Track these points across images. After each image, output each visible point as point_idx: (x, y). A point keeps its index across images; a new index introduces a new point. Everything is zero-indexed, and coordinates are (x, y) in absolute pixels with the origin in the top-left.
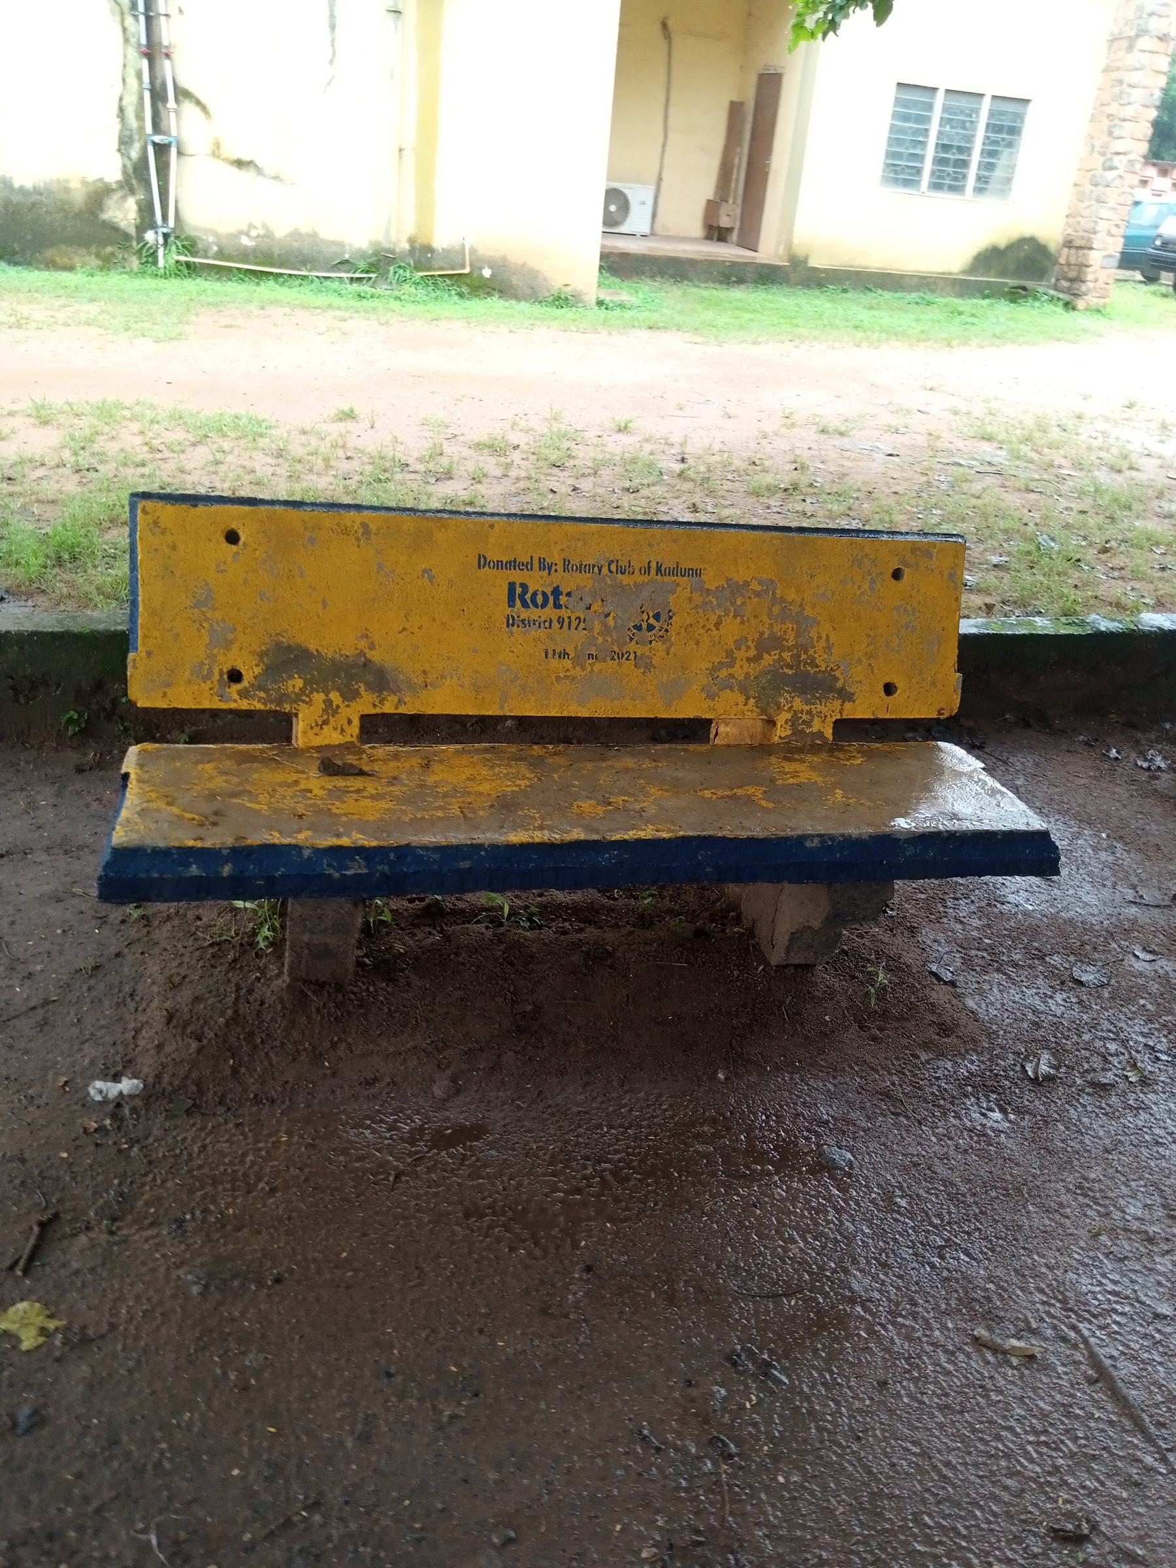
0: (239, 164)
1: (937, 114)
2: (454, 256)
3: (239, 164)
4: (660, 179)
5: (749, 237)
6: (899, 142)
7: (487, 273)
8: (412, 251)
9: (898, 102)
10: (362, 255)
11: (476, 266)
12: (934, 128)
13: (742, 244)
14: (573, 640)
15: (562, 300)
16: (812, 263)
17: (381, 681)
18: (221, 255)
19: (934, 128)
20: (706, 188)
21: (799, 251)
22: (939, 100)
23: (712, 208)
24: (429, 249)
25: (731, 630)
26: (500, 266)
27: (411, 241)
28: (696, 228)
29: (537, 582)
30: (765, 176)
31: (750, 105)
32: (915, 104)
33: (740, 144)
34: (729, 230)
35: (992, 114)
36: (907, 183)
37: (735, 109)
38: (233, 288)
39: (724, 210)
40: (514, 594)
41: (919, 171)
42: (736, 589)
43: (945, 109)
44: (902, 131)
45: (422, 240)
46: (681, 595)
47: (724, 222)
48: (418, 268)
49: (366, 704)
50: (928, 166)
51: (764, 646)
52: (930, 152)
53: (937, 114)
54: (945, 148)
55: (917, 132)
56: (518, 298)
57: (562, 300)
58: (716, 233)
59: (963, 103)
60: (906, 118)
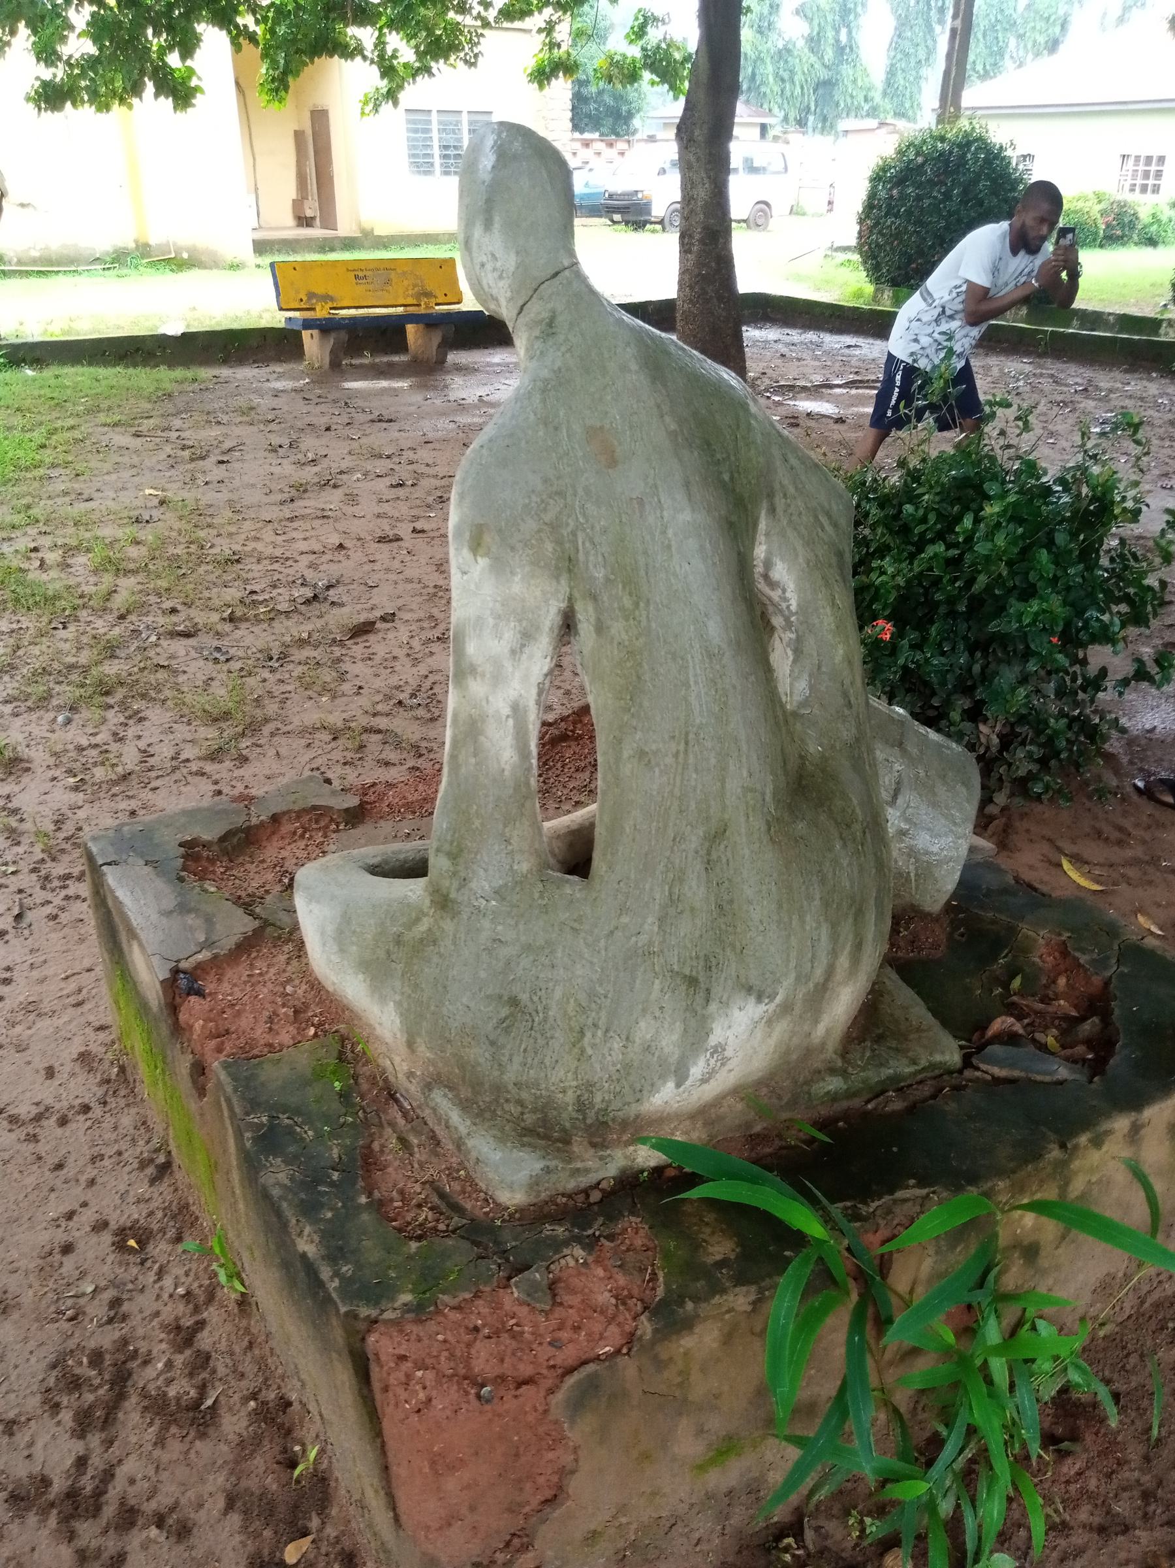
0: (22, 205)
1: (435, 126)
2: (164, 248)
3: (22, 205)
4: (256, 189)
5: (329, 220)
6: (414, 147)
7: (185, 256)
8: (137, 247)
9: (409, 121)
10: (107, 254)
11: (178, 251)
12: (435, 135)
13: (324, 226)
14: (371, 287)
15: (235, 267)
16: (376, 233)
17: (332, 299)
18: (19, 263)
19: (435, 135)
20: (290, 191)
21: (367, 225)
22: (434, 117)
23: (297, 205)
24: (147, 245)
25: (406, 283)
26: (192, 251)
27: (136, 242)
28: (290, 221)
29: (361, 274)
30: (331, 179)
31: (309, 132)
32: (420, 121)
33: (307, 158)
34: (313, 218)
35: (471, 123)
36: (426, 173)
37: (299, 136)
38: (34, 281)
39: (307, 204)
40: (356, 277)
41: (432, 165)
42: (404, 273)
43: (440, 123)
44: (414, 122)
45: (142, 241)
46: (393, 275)
47: (309, 213)
48: (143, 256)
49: (330, 305)
50: (437, 161)
51: (415, 286)
52: (436, 152)
53: (435, 126)
54: (446, 147)
55: (425, 139)
56: (205, 268)
57: (235, 267)
58: (304, 221)
59: (451, 118)
60: (416, 131)
